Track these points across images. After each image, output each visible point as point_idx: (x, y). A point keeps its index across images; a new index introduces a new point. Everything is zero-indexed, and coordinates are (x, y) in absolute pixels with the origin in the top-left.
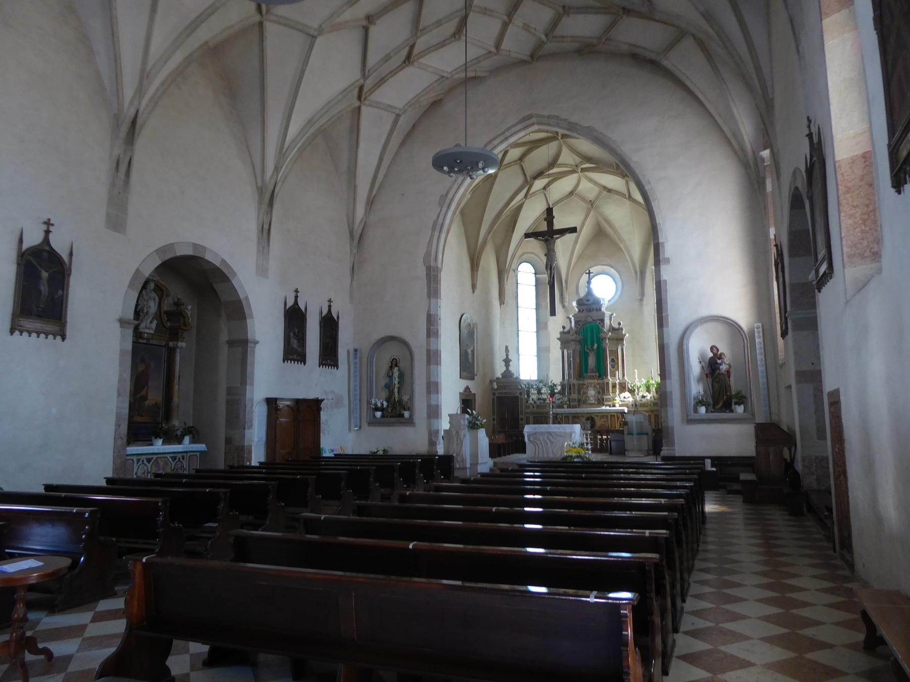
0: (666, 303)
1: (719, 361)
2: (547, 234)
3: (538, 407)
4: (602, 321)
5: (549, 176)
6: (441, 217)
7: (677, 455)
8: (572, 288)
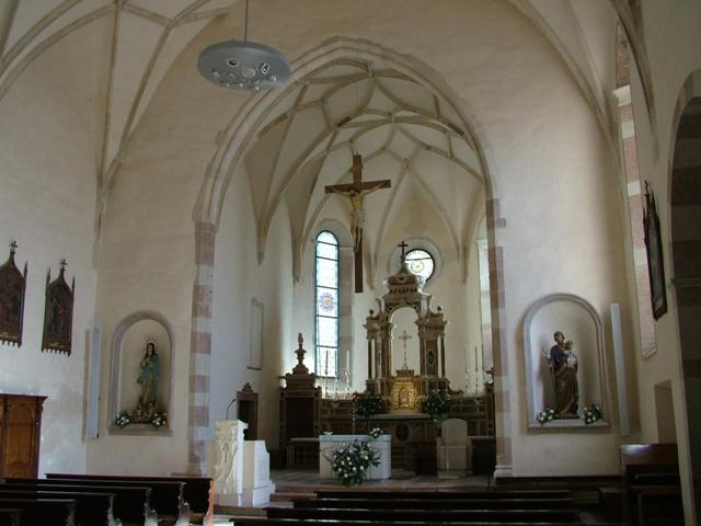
0: (502, 275)
1: (566, 352)
2: (354, 189)
5: (357, 124)
6: (218, 159)
7: (515, 475)
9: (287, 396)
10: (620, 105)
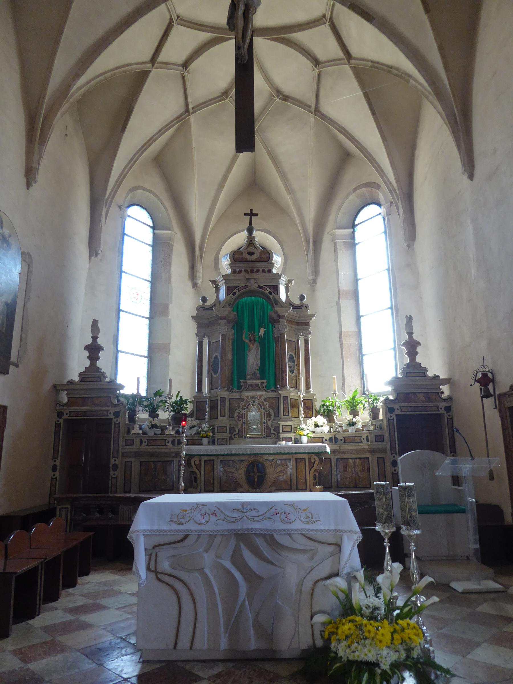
3: (151, 441)
4: (275, 289)
8: (209, 258)
9: (66, 417)
10: (143, 393)
